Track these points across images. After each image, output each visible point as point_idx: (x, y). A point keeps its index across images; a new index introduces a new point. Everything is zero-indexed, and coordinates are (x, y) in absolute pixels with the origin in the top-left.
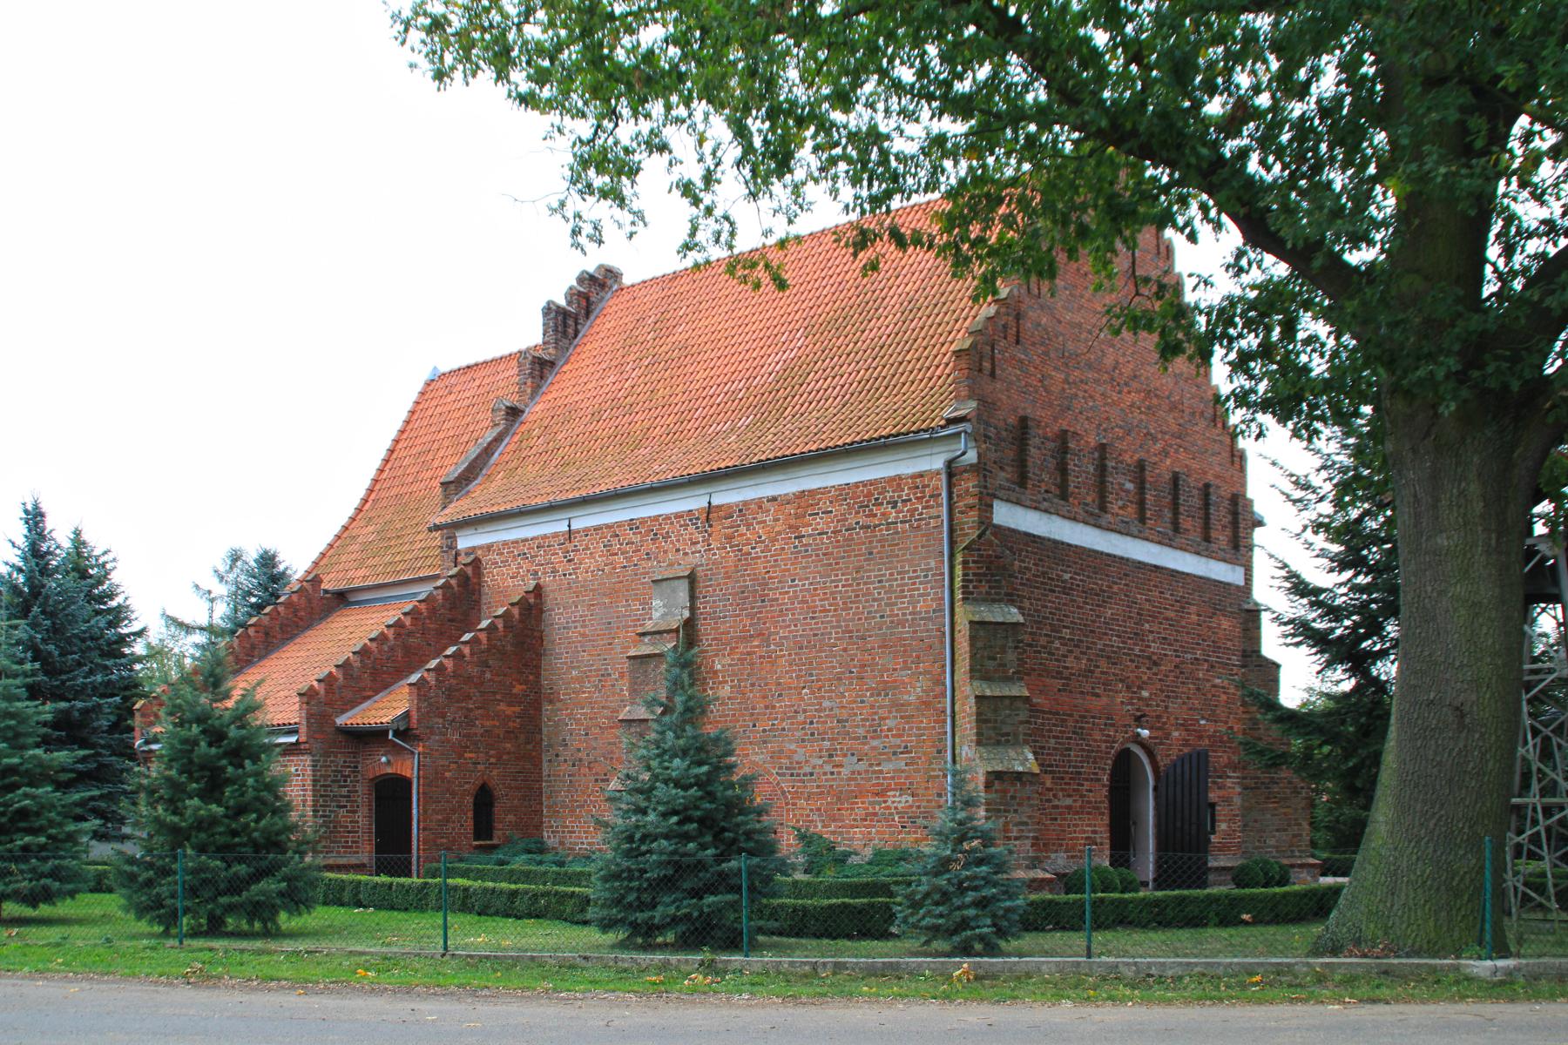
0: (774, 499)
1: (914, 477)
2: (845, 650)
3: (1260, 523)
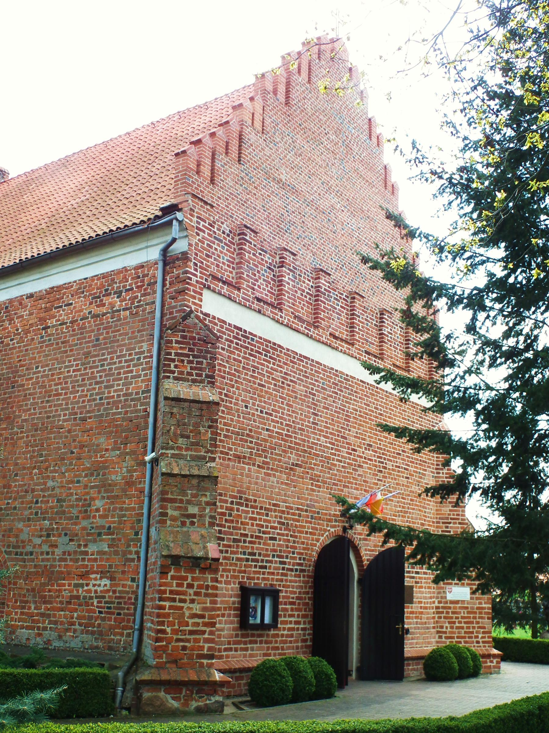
0: (31, 296)
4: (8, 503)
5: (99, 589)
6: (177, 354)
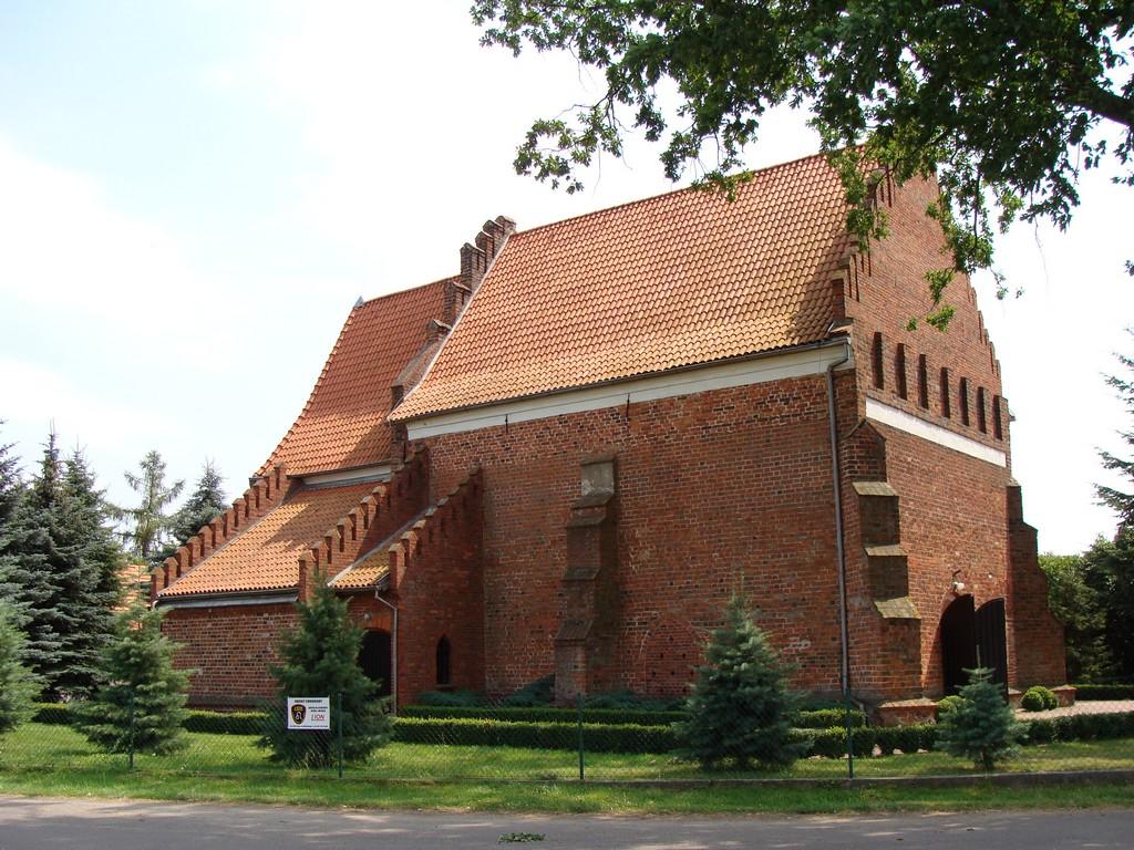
0: (684, 397)
1: (802, 379)
2: (749, 520)
3: (1013, 418)
4: (688, 583)
5: (800, 648)
6: (858, 457)
